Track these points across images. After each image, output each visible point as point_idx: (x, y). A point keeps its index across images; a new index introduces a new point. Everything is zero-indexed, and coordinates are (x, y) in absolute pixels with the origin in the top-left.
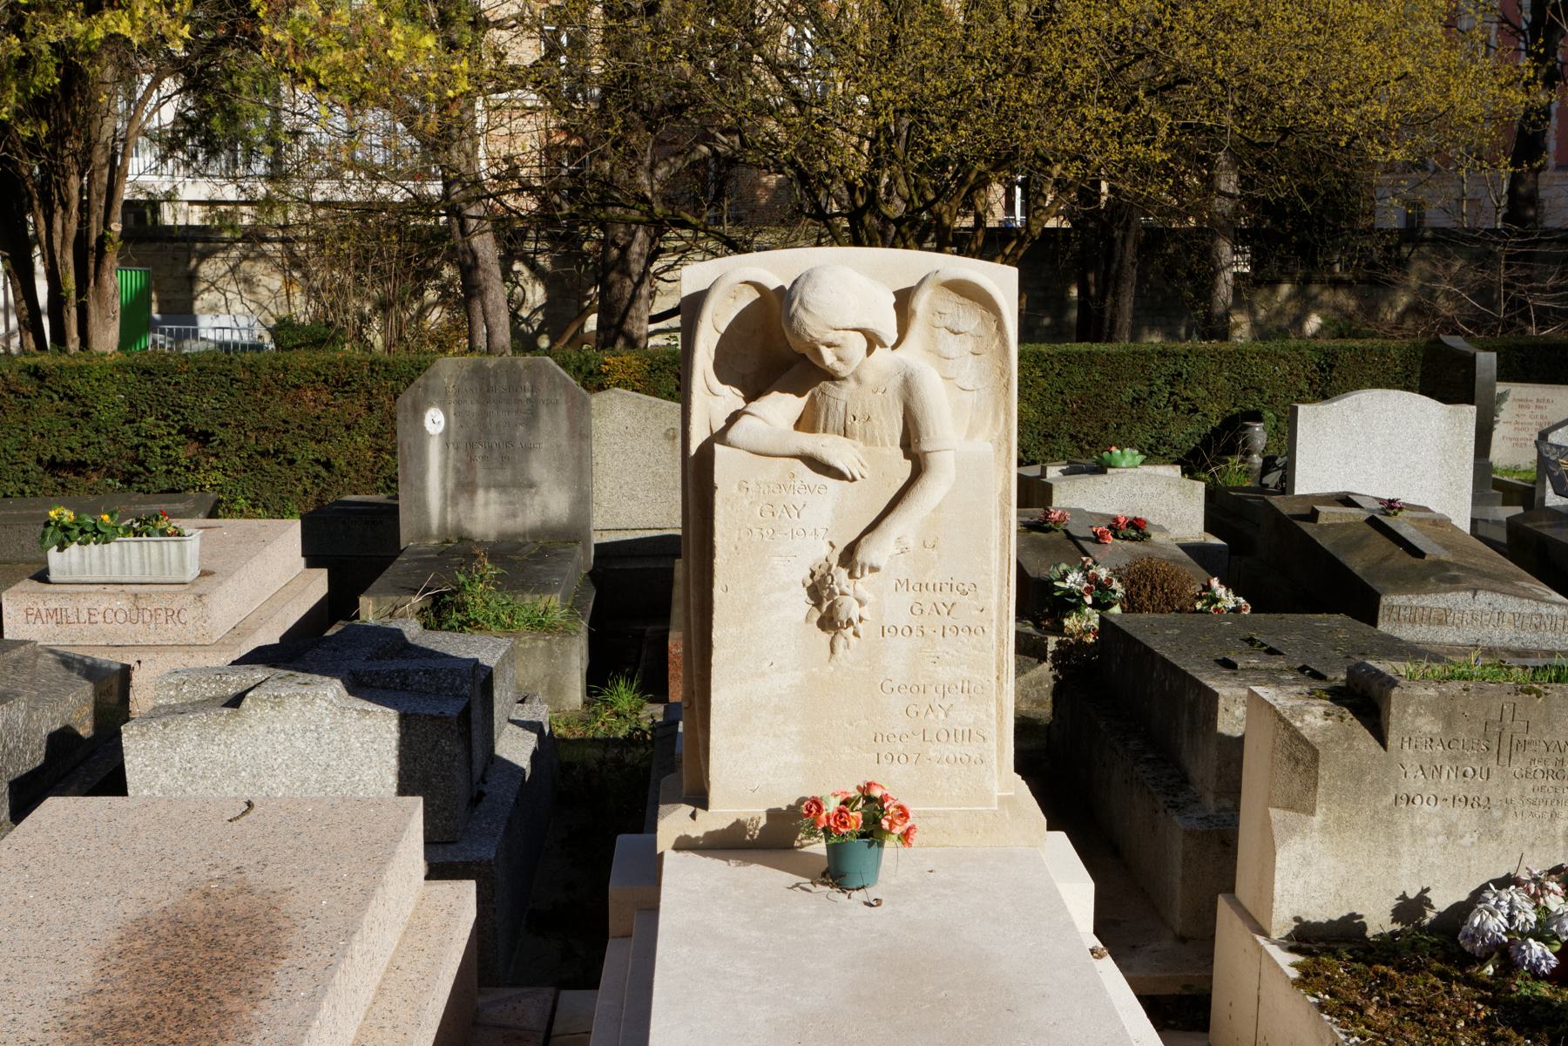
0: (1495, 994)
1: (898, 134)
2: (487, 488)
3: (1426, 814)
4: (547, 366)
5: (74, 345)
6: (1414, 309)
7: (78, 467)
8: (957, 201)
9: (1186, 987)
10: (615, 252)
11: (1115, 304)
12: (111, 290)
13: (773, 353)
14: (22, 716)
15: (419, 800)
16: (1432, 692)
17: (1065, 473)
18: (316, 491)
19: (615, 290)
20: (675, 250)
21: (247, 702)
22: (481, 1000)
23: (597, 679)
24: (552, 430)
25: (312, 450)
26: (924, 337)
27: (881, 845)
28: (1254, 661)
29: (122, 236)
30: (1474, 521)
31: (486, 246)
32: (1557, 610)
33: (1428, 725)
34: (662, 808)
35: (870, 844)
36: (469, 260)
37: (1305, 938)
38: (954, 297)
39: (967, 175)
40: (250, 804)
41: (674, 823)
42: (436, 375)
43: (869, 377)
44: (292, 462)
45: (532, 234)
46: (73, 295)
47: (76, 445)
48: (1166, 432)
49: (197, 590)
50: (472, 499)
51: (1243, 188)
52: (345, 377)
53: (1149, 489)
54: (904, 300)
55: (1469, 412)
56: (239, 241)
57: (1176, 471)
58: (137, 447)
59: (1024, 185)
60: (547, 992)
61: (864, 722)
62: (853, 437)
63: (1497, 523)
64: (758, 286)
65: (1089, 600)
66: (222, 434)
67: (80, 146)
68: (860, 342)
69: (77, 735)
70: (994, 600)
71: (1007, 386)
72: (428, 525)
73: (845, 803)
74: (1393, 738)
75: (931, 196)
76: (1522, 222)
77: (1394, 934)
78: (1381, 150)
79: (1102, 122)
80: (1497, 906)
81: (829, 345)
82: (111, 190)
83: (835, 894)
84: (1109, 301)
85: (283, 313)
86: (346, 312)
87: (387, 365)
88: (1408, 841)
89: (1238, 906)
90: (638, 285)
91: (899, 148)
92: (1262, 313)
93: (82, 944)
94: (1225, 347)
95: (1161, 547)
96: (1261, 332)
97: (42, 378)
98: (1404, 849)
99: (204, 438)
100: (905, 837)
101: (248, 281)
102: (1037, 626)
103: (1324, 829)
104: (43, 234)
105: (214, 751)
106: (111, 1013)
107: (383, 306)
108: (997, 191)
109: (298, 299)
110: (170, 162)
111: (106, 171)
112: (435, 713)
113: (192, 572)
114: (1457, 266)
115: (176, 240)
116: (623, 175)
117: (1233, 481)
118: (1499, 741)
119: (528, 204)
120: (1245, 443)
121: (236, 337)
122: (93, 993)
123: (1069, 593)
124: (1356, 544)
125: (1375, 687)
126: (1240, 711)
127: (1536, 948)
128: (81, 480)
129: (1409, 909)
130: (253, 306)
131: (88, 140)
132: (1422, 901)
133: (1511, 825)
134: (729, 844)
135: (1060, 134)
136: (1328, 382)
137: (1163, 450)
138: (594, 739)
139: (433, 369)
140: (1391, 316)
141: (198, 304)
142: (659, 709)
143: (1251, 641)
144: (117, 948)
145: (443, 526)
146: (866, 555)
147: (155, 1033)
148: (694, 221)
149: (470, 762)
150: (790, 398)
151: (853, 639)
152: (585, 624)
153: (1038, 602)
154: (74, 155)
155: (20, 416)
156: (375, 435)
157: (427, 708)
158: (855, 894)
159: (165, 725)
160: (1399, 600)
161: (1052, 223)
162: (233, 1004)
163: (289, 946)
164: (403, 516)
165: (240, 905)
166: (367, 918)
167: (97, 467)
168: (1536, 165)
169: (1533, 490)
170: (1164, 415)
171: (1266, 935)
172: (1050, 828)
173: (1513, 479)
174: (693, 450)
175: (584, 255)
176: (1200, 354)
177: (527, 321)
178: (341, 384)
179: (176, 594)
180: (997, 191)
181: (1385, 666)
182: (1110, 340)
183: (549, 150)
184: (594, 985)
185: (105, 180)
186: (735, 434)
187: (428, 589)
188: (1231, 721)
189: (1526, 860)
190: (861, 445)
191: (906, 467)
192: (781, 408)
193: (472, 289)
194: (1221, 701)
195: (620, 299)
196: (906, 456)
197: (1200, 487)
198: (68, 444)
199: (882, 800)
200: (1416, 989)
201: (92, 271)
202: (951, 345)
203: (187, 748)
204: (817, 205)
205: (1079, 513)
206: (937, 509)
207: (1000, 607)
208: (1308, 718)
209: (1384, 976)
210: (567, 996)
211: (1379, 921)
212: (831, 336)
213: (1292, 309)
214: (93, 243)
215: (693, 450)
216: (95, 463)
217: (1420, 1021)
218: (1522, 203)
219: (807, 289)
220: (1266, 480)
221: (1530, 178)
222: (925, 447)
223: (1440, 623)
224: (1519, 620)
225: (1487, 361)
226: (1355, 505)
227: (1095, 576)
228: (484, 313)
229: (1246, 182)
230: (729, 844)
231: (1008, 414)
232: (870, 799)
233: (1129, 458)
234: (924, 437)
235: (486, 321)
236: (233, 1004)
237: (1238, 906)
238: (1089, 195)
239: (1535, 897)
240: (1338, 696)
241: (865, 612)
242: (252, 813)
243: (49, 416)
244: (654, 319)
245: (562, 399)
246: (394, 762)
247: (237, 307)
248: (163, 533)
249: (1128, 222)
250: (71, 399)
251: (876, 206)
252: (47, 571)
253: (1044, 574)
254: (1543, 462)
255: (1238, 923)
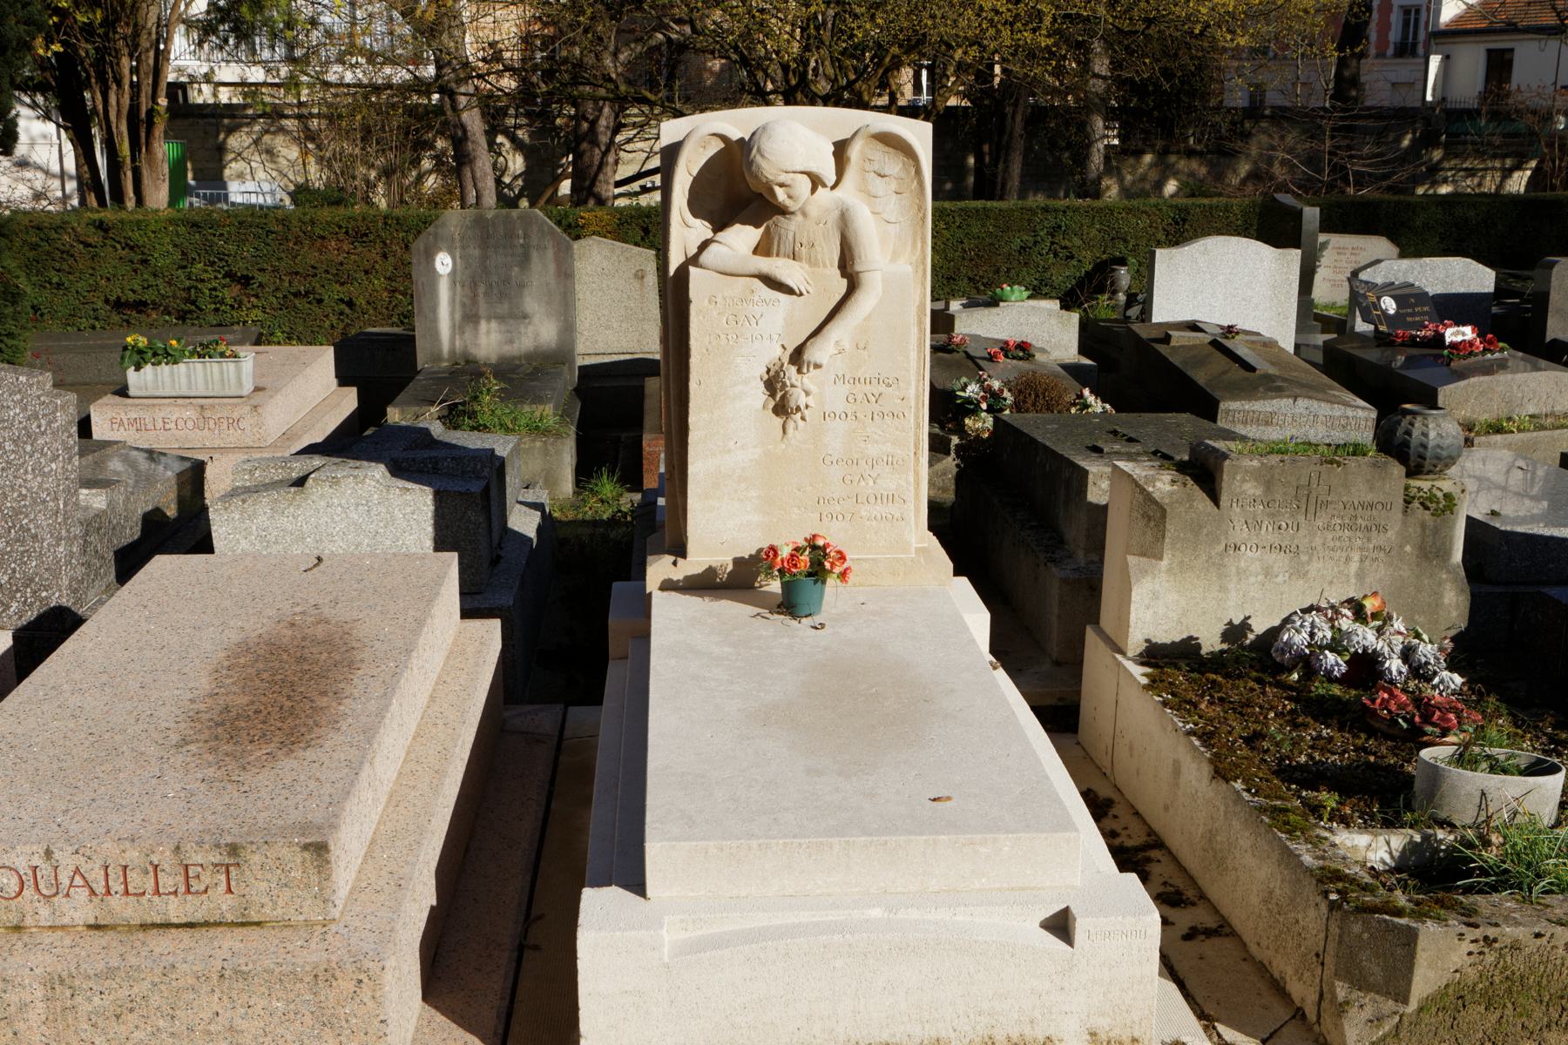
0: (1299, 694)
1: (824, 23)
2: (489, 319)
3: (1249, 558)
4: (536, 216)
5: (130, 204)
6: (1255, 176)
7: (140, 306)
8: (874, 82)
9: (1060, 699)
10: (585, 125)
11: (1006, 169)
12: (160, 156)
13: (736, 192)
14: (122, 498)
15: (456, 554)
16: (1255, 463)
17: (965, 306)
18: (341, 326)
19: (586, 158)
20: (634, 125)
21: (310, 481)
22: (506, 714)
23: (585, 472)
24: (542, 269)
25: (334, 292)
26: (855, 178)
27: (824, 582)
28: (1117, 447)
29: (168, 109)
30: (1297, 346)
31: (473, 121)
32: (1360, 413)
33: (1252, 489)
34: (650, 558)
35: (816, 582)
36: (460, 133)
37: (1154, 655)
38: (881, 146)
39: (881, 60)
40: (319, 559)
41: (659, 569)
42: (444, 225)
43: (813, 211)
44: (320, 301)
45: (512, 111)
46: (128, 160)
47: (136, 287)
48: (1047, 275)
49: (253, 402)
50: (476, 329)
51: (1112, 70)
52: (363, 229)
53: (1034, 319)
54: (841, 149)
55: (1295, 255)
56: (260, 116)
57: (1054, 305)
58: (189, 289)
59: (930, 69)
60: (559, 708)
61: (809, 488)
62: (800, 260)
63: (1316, 347)
64: (723, 138)
65: (984, 406)
66: (260, 278)
67: (129, 31)
68: (806, 183)
69: (164, 514)
70: (912, 392)
71: (923, 219)
72: (440, 350)
73: (797, 549)
74: (1224, 499)
75: (852, 77)
76: (1345, 99)
77: (1222, 652)
78: (1229, 37)
79: (997, 12)
80: (1302, 626)
81: (781, 185)
82: (157, 72)
83: (787, 619)
84: (1001, 166)
85: (301, 180)
86: (354, 178)
87: (398, 219)
88: (1235, 579)
89: (1101, 633)
90: (605, 154)
91: (826, 35)
92: (1129, 177)
93: (197, 661)
94: (1097, 204)
95: (1043, 365)
96: (1126, 192)
97: (106, 231)
98: (1231, 586)
99: (245, 281)
100: (843, 575)
101: (270, 152)
102: (942, 428)
103: (1169, 570)
104: (100, 107)
105: (284, 522)
106: (227, 709)
107: (387, 173)
108: (906, 74)
109: (313, 168)
110: (206, 46)
111: (152, 54)
112: (463, 490)
113: (248, 387)
114: (1289, 139)
115: (206, 116)
116: (590, 60)
117: (1103, 314)
118: (1307, 501)
119: (509, 83)
120: (1112, 284)
121: (261, 200)
122: (211, 696)
123: (968, 401)
124: (1200, 362)
125: (1212, 460)
126: (1105, 485)
127: (1331, 657)
128: (143, 317)
129: (1235, 632)
130: (274, 174)
131: (136, 25)
132: (1245, 626)
133: (1315, 566)
134: (704, 585)
135: (963, 23)
136: (1181, 230)
137: (1045, 290)
138: (584, 521)
139: (442, 219)
140: (1235, 181)
141: (227, 172)
142: (637, 497)
143: (1115, 433)
144: (226, 664)
145: (452, 352)
146: (812, 354)
147: (264, 722)
148: (652, 97)
149: (490, 531)
150: (749, 229)
151: (801, 423)
152: (573, 428)
153: (946, 409)
154: (125, 38)
155: (89, 263)
156: (389, 279)
157: (456, 486)
158: (804, 620)
159: (244, 501)
160: (1234, 405)
161: (953, 102)
162: (323, 702)
163: (362, 661)
164: (421, 344)
165: (320, 632)
166: (421, 641)
167: (156, 306)
168: (1357, 50)
169: (1344, 322)
170: (1046, 261)
171: (1123, 653)
172: (956, 574)
173: (1331, 313)
174: (672, 271)
175: (557, 129)
176: (1076, 210)
177: (509, 186)
178: (359, 234)
179: (236, 405)
180: (906, 74)
181: (1220, 445)
182: (1001, 198)
183: (527, 39)
184: (599, 702)
185: (151, 61)
186: (705, 258)
187: (443, 401)
188: (1098, 491)
189: (1326, 594)
190: (807, 266)
191: (845, 282)
192: (742, 237)
193: (463, 157)
194: (1090, 476)
195: (590, 166)
196: (843, 275)
197: (1075, 317)
198: (130, 287)
199: (825, 547)
200: (1238, 691)
201: (143, 140)
202: (879, 186)
203: (262, 520)
204: (757, 84)
205: (976, 338)
206: (868, 318)
207: (917, 397)
208: (1158, 484)
209: (1214, 682)
210: (577, 713)
211: (1211, 642)
212: (783, 178)
213: (1154, 175)
214: (143, 115)
215: (672, 271)
216: (154, 303)
217: (1241, 714)
218: (1346, 85)
219: (764, 140)
220: (1129, 313)
221: (1354, 63)
222: (858, 268)
223: (1267, 423)
224: (1330, 421)
225: (1312, 214)
226: (1201, 330)
227: (990, 387)
228: (474, 178)
229: (1116, 65)
230: (704, 585)
231: (924, 242)
232: (814, 548)
233: (1017, 294)
234: (857, 261)
235: (475, 185)
236: (323, 702)
237: (1101, 633)
238: (985, 75)
239: (1331, 620)
240: (1182, 468)
241: (811, 401)
242: (322, 566)
243: (114, 262)
244: (618, 184)
245: (549, 244)
246: (430, 529)
247: (261, 175)
248: (222, 355)
249: (1017, 100)
250: (132, 248)
251: (807, 85)
252: (126, 387)
253: (948, 386)
254: (1355, 298)
255: (1101, 645)
